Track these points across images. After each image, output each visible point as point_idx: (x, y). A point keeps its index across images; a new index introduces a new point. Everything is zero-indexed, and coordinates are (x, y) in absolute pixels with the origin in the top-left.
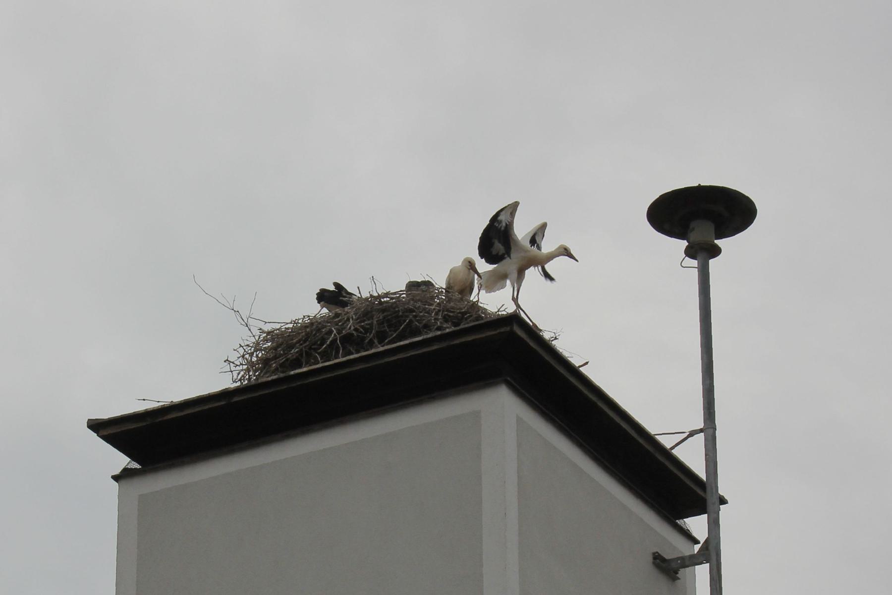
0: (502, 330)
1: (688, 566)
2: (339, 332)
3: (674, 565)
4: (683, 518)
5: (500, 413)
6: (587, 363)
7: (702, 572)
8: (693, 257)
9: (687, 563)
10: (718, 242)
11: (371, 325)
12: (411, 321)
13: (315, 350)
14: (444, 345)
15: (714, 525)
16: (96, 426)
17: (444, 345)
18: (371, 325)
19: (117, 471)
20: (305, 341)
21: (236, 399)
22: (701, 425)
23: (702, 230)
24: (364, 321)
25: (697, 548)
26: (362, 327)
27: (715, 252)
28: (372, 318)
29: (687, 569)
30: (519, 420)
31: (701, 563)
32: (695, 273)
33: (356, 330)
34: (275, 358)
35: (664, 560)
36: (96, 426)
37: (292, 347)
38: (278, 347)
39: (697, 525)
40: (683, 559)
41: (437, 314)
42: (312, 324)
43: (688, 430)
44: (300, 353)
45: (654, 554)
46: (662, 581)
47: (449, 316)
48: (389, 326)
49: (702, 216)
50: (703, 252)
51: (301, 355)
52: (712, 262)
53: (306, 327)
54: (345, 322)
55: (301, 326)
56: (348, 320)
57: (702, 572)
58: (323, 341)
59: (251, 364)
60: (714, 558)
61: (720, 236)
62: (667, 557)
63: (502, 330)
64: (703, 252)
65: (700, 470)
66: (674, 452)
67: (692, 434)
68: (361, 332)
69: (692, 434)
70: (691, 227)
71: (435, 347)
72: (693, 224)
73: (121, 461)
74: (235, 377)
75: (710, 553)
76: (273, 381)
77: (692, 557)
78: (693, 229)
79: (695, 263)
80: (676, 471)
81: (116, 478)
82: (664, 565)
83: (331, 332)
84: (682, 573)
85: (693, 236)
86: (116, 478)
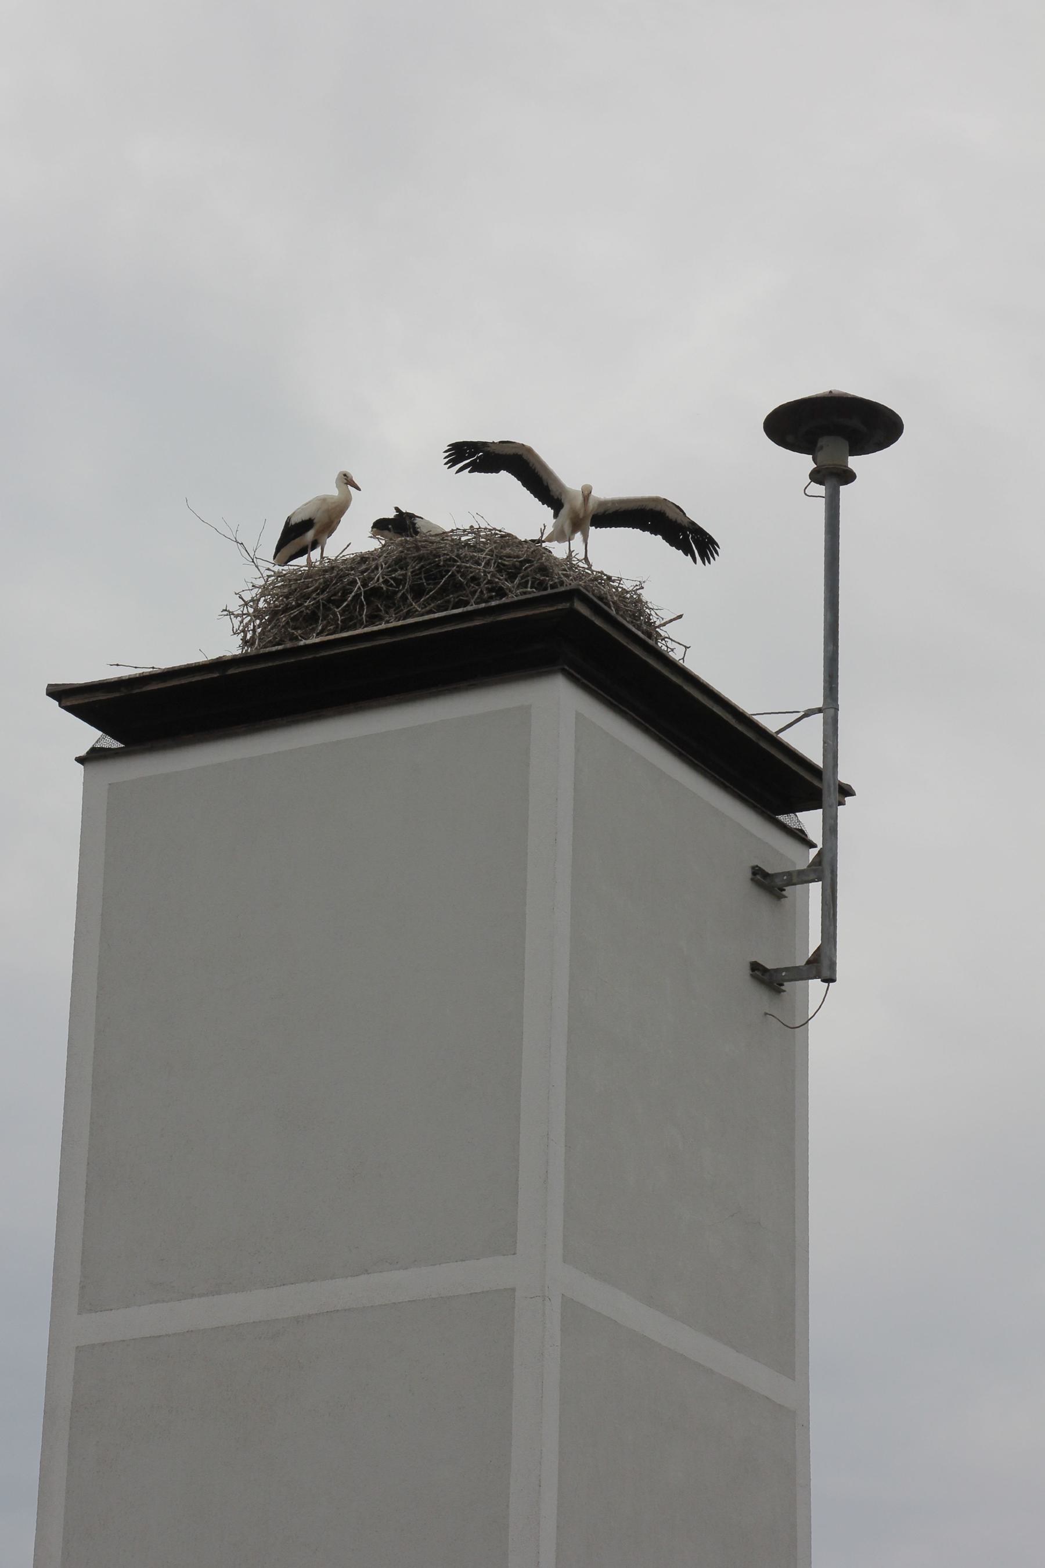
0: (560, 607)
1: (795, 884)
2: (364, 585)
3: (778, 882)
4: (794, 811)
5: (556, 708)
6: (680, 617)
7: (815, 889)
8: (820, 482)
9: (795, 880)
10: (854, 463)
11: (405, 575)
12: (453, 575)
13: (334, 602)
14: (489, 620)
15: (830, 829)
16: (60, 694)
17: (489, 620)
18: (405, 575)
19: (83, 753)
20: (323, 591)
21: (230, 672)
22: (820, 704)
23: (830, 445)
24: (396, 571)
25: (813, 853)
26: (394, 579)
27: (848, 477)
28: (407, 565)
29: (798, 886)
30: (579, 716)
31: (813, 881)
32: (821, 505)
33: (386, 582)
34: (286, 610)
35: (766, 875)
36: (60, 694)
37: (307, 597)
38: (290, 594)
39: (810, 821)
40: (789, 874)
41: (488, 564)
42: (332, 568)
43: (803, 708)
44: (317, 605)
45: (753, 868)
46: (762, 901)
47: (504, 565)
48: (427, 579)
49: (832, 430)
50: (833, 476)
51: (318, 607)
52: (843, 489)
53: (325, 571)
54: (373, 571)
55: (319, 570)
56: (376, 568)
57: (815, 889)
58: (346, 592)
59: (258, 614)
60: (828, 874)
61: (853, 453)
62: (770, 871)
63: (560, 607)
64: (833, 476)
65: (815, 755)
66: (781, 736)
67: (808, 713)
68: (391, 585)
69: (808, 713)
70: (819, 444)
71: (477, 623)
72: (822, 441)
73: (89, 736)
74: (236, 627)
75: (824, 869)
76: (277, 652)
77: (800, 872)
78: (822, 448)
79: (820, 490)
80: (786, 761)
81: (80, 760)
82: (766, 882)
83: (354, 582)
84: (789, 890)
85: (820, 455)
86: (80, 760)
